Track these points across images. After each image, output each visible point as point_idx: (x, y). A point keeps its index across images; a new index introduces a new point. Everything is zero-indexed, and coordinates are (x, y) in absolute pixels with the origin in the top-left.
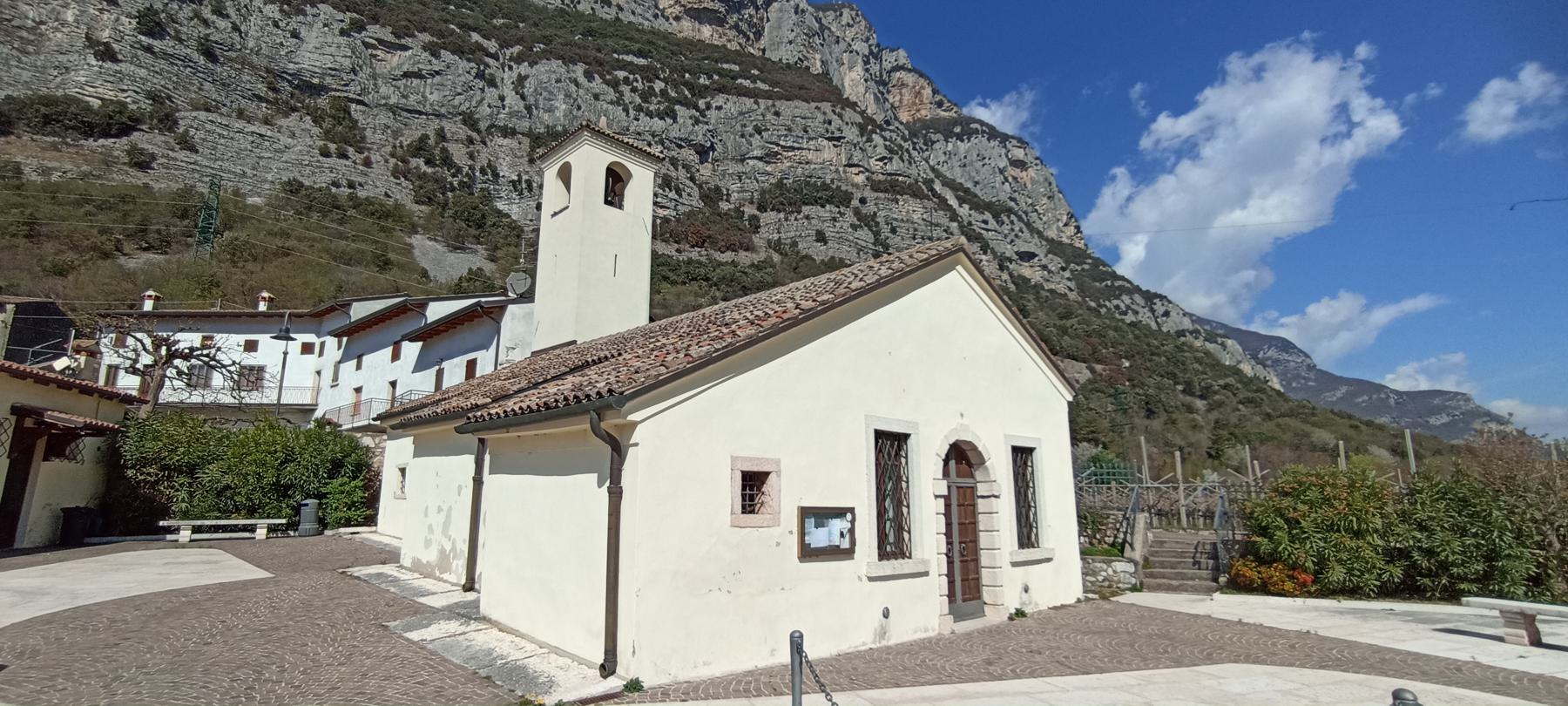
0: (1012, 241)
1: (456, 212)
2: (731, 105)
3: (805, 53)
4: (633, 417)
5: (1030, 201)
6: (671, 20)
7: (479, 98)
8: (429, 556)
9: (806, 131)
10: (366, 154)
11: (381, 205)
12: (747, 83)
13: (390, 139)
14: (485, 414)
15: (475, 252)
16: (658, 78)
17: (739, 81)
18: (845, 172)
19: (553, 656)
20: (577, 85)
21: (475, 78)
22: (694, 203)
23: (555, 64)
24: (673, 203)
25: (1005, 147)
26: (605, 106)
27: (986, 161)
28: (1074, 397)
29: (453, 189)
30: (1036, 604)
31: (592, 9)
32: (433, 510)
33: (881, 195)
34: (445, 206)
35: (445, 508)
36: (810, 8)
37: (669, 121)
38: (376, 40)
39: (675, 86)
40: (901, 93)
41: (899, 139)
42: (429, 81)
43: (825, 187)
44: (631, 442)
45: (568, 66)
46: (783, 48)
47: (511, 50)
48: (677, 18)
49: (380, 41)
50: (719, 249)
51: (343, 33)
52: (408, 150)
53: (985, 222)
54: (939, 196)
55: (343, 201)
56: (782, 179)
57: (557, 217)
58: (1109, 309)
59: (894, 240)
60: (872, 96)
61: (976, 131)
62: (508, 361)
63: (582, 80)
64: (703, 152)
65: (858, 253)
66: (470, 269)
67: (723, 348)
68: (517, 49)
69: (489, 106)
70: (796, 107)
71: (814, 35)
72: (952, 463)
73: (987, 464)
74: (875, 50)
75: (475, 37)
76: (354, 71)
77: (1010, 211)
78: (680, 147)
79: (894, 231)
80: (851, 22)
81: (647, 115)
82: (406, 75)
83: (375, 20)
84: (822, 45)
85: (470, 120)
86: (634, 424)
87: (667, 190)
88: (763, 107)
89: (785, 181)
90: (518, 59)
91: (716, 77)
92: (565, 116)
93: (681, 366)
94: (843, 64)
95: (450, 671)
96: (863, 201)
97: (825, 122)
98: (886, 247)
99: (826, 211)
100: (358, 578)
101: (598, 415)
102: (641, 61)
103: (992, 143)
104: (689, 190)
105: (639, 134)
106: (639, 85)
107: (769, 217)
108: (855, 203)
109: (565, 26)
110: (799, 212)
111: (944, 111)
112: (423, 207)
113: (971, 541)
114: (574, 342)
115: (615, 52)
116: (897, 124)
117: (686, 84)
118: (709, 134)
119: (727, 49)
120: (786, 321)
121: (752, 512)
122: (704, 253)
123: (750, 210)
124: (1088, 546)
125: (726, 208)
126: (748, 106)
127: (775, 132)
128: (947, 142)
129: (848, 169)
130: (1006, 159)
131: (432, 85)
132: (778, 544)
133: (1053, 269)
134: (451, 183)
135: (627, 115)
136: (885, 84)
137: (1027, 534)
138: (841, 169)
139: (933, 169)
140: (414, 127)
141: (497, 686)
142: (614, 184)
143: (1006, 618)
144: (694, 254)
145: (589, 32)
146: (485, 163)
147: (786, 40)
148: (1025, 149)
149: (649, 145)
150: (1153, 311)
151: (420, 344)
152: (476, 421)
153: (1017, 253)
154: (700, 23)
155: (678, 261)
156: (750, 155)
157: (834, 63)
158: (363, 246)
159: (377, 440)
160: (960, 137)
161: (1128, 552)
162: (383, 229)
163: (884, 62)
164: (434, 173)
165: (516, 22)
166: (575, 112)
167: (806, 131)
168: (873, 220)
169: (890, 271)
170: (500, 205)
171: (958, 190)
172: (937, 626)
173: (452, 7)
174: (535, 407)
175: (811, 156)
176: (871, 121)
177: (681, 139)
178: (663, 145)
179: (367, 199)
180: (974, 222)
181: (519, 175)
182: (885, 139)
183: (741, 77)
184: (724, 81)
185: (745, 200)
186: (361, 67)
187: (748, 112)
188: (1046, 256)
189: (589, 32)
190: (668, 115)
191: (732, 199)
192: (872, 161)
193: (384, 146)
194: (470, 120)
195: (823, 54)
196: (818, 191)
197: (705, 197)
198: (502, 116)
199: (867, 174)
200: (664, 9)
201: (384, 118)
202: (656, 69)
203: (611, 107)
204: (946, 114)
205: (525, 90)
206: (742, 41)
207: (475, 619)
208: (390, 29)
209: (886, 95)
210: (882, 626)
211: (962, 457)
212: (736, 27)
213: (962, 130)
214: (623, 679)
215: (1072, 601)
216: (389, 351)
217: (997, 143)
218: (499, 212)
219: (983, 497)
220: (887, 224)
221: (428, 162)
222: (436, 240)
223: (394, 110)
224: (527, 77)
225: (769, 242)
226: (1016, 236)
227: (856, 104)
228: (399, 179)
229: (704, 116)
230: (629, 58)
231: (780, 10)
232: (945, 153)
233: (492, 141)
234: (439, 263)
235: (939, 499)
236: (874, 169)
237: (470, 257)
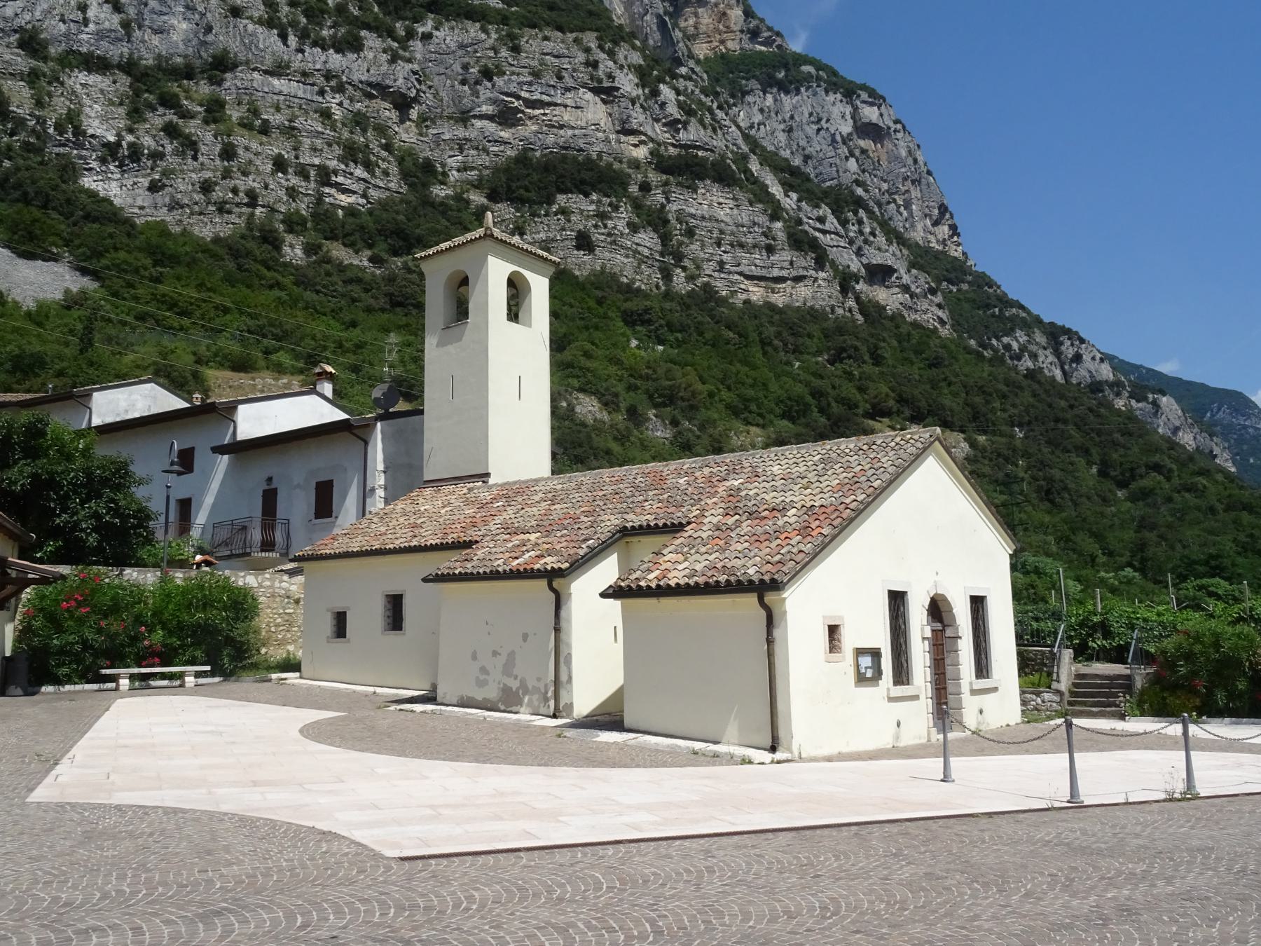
5: (885, 186)
9: (560, 78)
22: (392, 185)
25: (851, 103)
26: (251, 27)
41: (697, 91)
53: (821, 220)
54: (755, 181)
56: (525, 150)
58: (995, 350)
66: (67, 291)
77: (859, 203)
78: (370, 97)
86: (785, 599)
88: (494, 36)
96: (645, 187)
103: (831, 97)
104: (384, 165)
108: (634, 189)
111: (761, 44)
116: (692, 64)
129: (623, 138)
133: (918, 291)
137: (982, 669)
148: (879, 107)
149: (322, 93)
150: (1058, 353)
153: (867, 267)
156: (476, 111)
160: (784, 87)
161: (1055, 685)
167: (560, 78)
170: (88, 182)
175: (567, 116)
177: (370, 84)
180: (805, 220)
181: (118, 135)
182: (678, 93)
187: (472, 44)
188: (909, 271)
203: (260, 29)
211: (938, 610)
213: (786, 76)
220: (681, 223)
226: (866, 241)
232: (761, 110)
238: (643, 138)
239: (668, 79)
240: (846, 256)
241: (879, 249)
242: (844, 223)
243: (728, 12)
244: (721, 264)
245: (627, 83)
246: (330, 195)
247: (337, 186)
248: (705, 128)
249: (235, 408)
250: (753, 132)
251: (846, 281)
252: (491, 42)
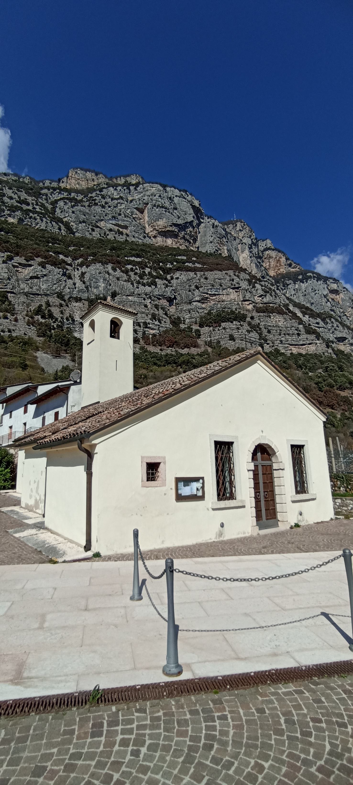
0: (333, 332)
1: (56, 340)
2: (182, 276)
3: (219, 247)
4: (94, 442)
5: (342, 310)
6: (152, 238)
7: (64, 285)
8: (31, 502)
9: (221, 286)
10: (15, 316)
11: (22, 339)
12: (190, 265)
13: (25, 308)
14: (43, 441)
15: (65, 357)
16: (147, 267)
17: (186, 264)
18: (242, 304)
19: (69, 543)
20: (109, 274)
21: (62, 276)
22: (167, 326)
23: (98, 265)
24: (157, 327)
25: (327, 284)
26: (122, 283)
27: (317, 292)
28: (327, 419)
29: (54, 329)
30: (307, 520)
31: (114, 237)
32: (32, 482)
33: (262, 314)
34: (51, 336)
35: (37, 481)
36: (220, 224)
37: (153, 287)
38: (18, 263)
39: (155, 270)
40: (269, 262)
41: (269, 285)
42: (41, 279)
43: (232, 312)
44: (95, 452)
45: (104, 266)
46: (207, 246)
47: (78, 261)
48: (155, 237)
49: (20, 264)
50: (181, 348)
51: (4, 262)
52: (33, 312)
53: (318, 323)
55: (6, 339)
56: (210, 310)
57: (90, 345)
59: (270, 337)
60: (254, 265)
61: (310, 277)
62: (72, 412)
63: (111, 271)
64: (170, 301)
65: (251, 345)
66: (63, 366)
67: (135, 410)
68: (80, 260)
69: (69, 288)
70: (216, 274)
71: (223, 238)
72: (259, 454)
73: (277, 454)
74: (255, 241)
75: (61, 257)
76: (9, 279)
77: (331, 317)
78: (159, 299)
79: (269, 332)
80: (241, 229)
81: (142, 285)
82: (32, 278)
83: (17, 254)
84: (227, 242)
85: (60, 296)
86: (95, 445)
87: (154, 320)
88: (199, 275)
89: (212, 311)
90: (81, 265)
91: (175, 263)
92: (104, 289)
93: (115, 419)
94: (238, 250)
95: (26, 549)
96: (252, 318)
97: (230, 280)
98: (266, 340)
99: (233, 325)
100: (3, 512)
101: (81, 442)
102: (139, 260)
103: (319, 282)
104: (165, 320)
105: (139, 295)
106: (138, 271)
107: (205, 330)
108: (248, 319)
109: (102, 247)
110: (220, 326)
111: (293, 268)
112: (41, 338)
113: (270, 491)
114: (99, 402)
115: (126, 256)
116: (268, 277)
117: (161, 268)
118: (173, 292)
119: (180, 249)
120: (166, 395)
121: (154, 480)
122: (174, 350)
123: (195, 327)
124: (345, 492)
125: (183, 327)
126: (192, 276)
127: (206, 288)
128: (295, 284)
129: (244, 303)
130: (327, 290)
131: (43, 281)
132: (165, 494)
134: (53, 326)
135: (133, 286)
136: (261, 258)
138: (240, 303)
139: (288, 298)
140: (36, 302)
141: (42, 554)
142: (115, 327)
143: (288, 528)
144: (169, 351)
145: (113, 249)
146: (68, 315)
147: (209, 241)
148: (337, 284)
151: (35, 405)
152: (40, 444)
154: (166, 238)
155: (161, 355)
157: (234, 250)
158: (14, 359)
159: (16, 451)
162: (23, 350)
163: (259, 247)
164: (45, 322)
165: (80, 248)
166: (108, 287)
167: (221, 286)
168: (258, 327)
169: (220, 367)
171: (302, 308)
172: (250, 531)
173: (50, 244)
174: (60, 438)
175: (224, 298)
176: (254, 277)
177: (159, 295)
178: (151, 299)
179: (16, 337)
180: (312, 324)
182: (262, 286)
183: (187, 262)
184: (179, 265)
185: (193, 322)
186: (12, 276)
187: (192, 279)
189: (113, 249)
190: (152, 284)
191: (186, 322)
192: (256, 298)
193: (23, 311)
194: (60, 296)
195: (228, 246)
196: (229, 315)
197: (173, 323)
198: (75, 292)
199: (254, 304)
200: (148, 233)
201: (23, 299)
202: (146, 263)
203: (125, 283)
204: (294, 270)
205: (85, 279)
206: (187, 244)
207: (43, 529)
208: (23, 258)
209: (262, 263)
210: (220, 531)
212: (184, 238)
213: (302, 277)
214: (93, 552)
215: (328, 519)
216: (22, 409)
217: (322, 282)
218: (75, 338)
219: (276, 470)
220: (266, 329)
221: (43, 317)
222: (47, 353)
223: (27, 294)
224: (85, 273)
225: (206, 342)
226: (335, 329)
227: (246, 269)
228: (30, 326)
229: (170, 283)
230: (133, 259)
231: (205, 227)
232: (294, 290)
233: (71, 304)
234: (49, 364)
235: (250, 472)
236: (257, 302)
237: (63, 360)
238: (250, 302)
239: (258, 282)
240: (328, 335)
241: (340, 332)
242: (326, 323)
243: (280, 259)
244: (281, 341)
245: (244, 285)
246: (147, 331)
247: (149, 328)
248: (272, 296)
249: (38, 387)
250: (292, 297)
251: (328, 344)
252: (197, 278)
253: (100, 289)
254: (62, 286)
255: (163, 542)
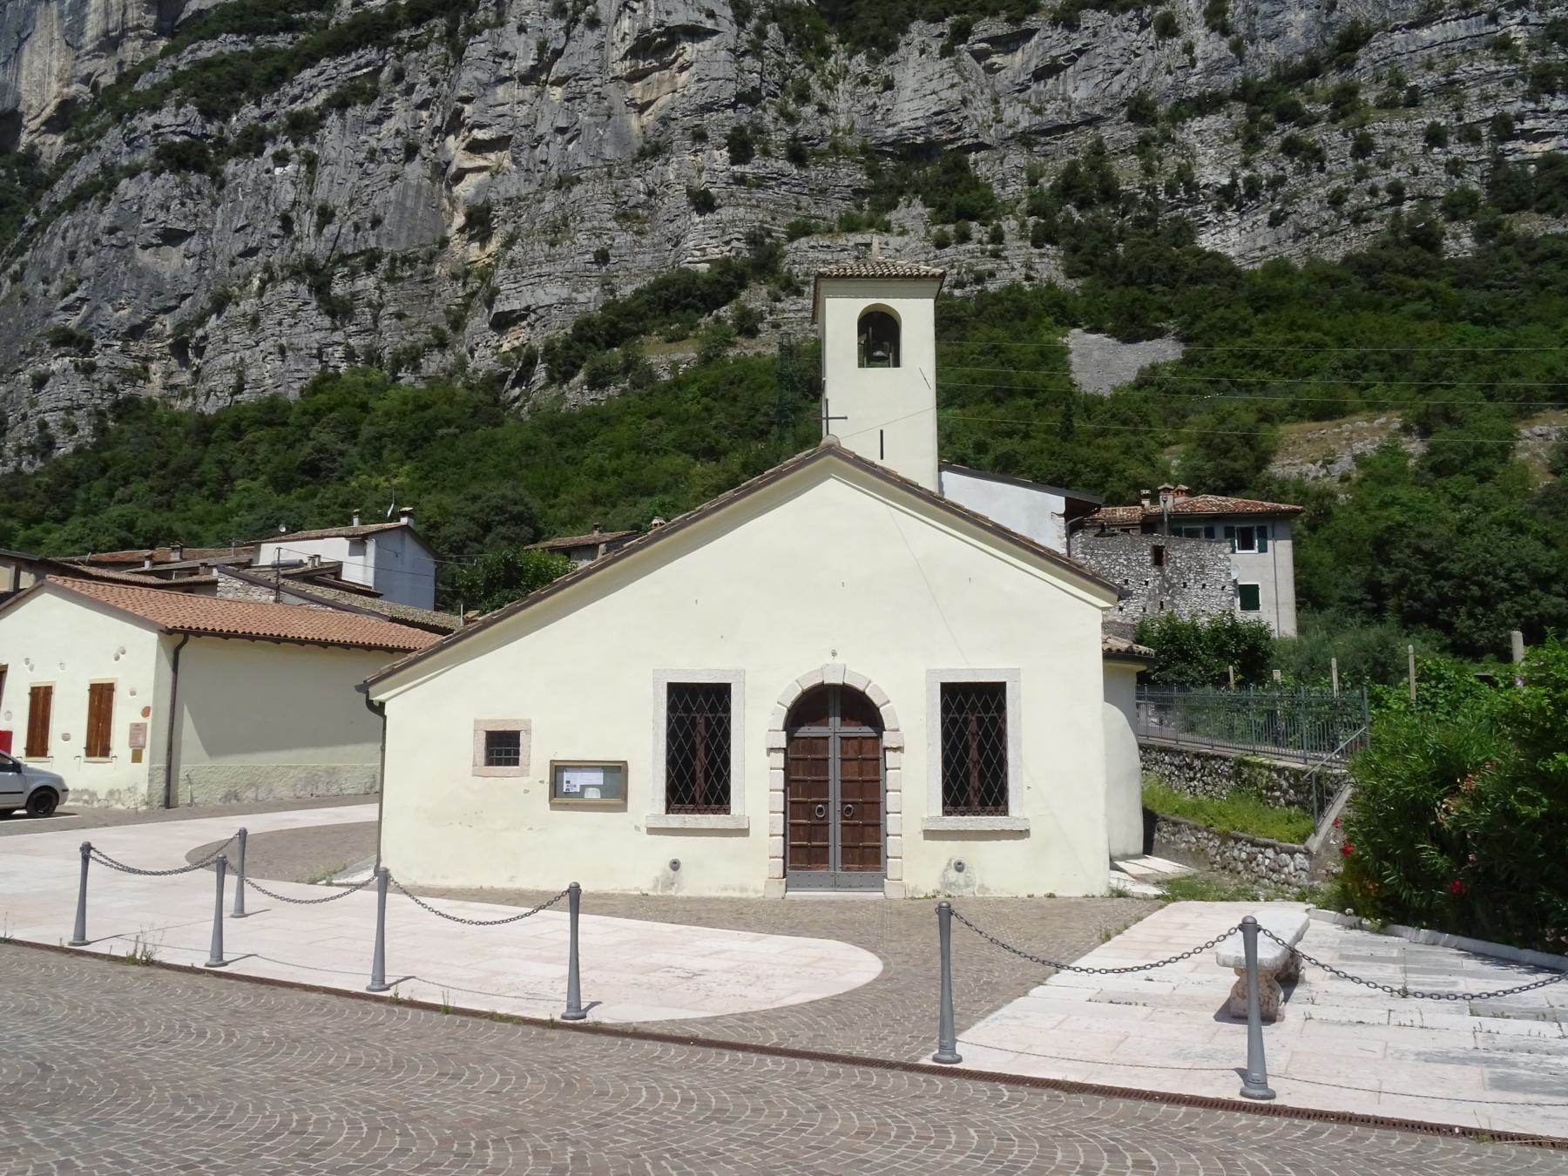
49: (993, 40)
87: (1547, 97)
201: (1016, 158)
223: (1026, 140)
246: (1514, 151)
253: (1293, 34)
254: (1144, 70)
255: (512, 878)
